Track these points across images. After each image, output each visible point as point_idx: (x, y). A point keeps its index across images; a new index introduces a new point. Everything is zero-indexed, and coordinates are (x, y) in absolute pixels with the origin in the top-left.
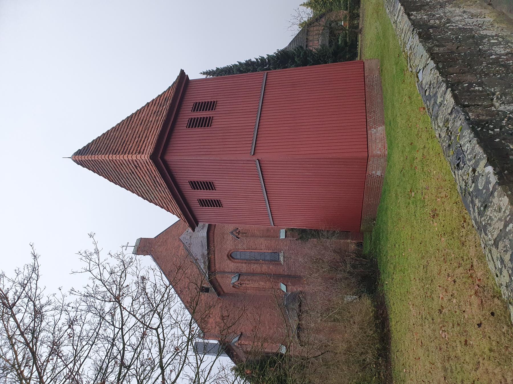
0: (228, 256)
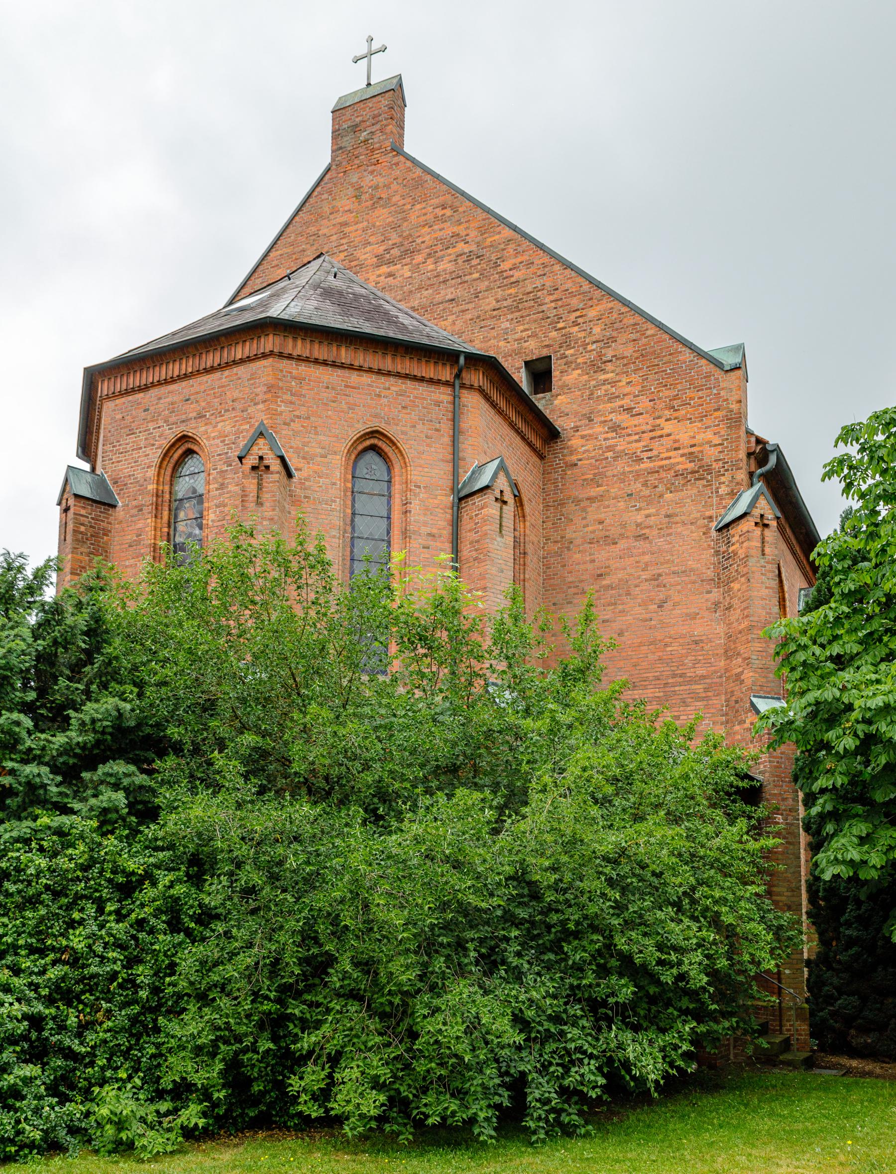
0: (184, 438)
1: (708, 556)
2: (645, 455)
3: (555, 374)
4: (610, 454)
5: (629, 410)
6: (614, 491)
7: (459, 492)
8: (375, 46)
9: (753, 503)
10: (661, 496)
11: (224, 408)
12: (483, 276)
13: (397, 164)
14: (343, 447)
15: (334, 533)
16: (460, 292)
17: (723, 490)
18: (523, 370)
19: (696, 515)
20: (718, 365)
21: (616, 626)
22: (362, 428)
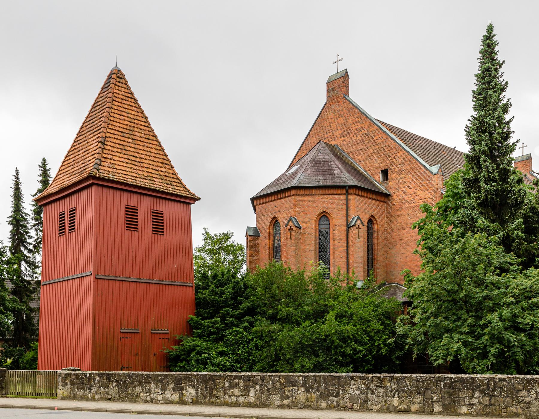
0: (275, 217)
4: (403, 201)
8: (339, 59)
11: (284, 209)
12: (370, 142)
15: (313, 242)
16: (363, 147)
21: (405, 255)
22: (320, 211)
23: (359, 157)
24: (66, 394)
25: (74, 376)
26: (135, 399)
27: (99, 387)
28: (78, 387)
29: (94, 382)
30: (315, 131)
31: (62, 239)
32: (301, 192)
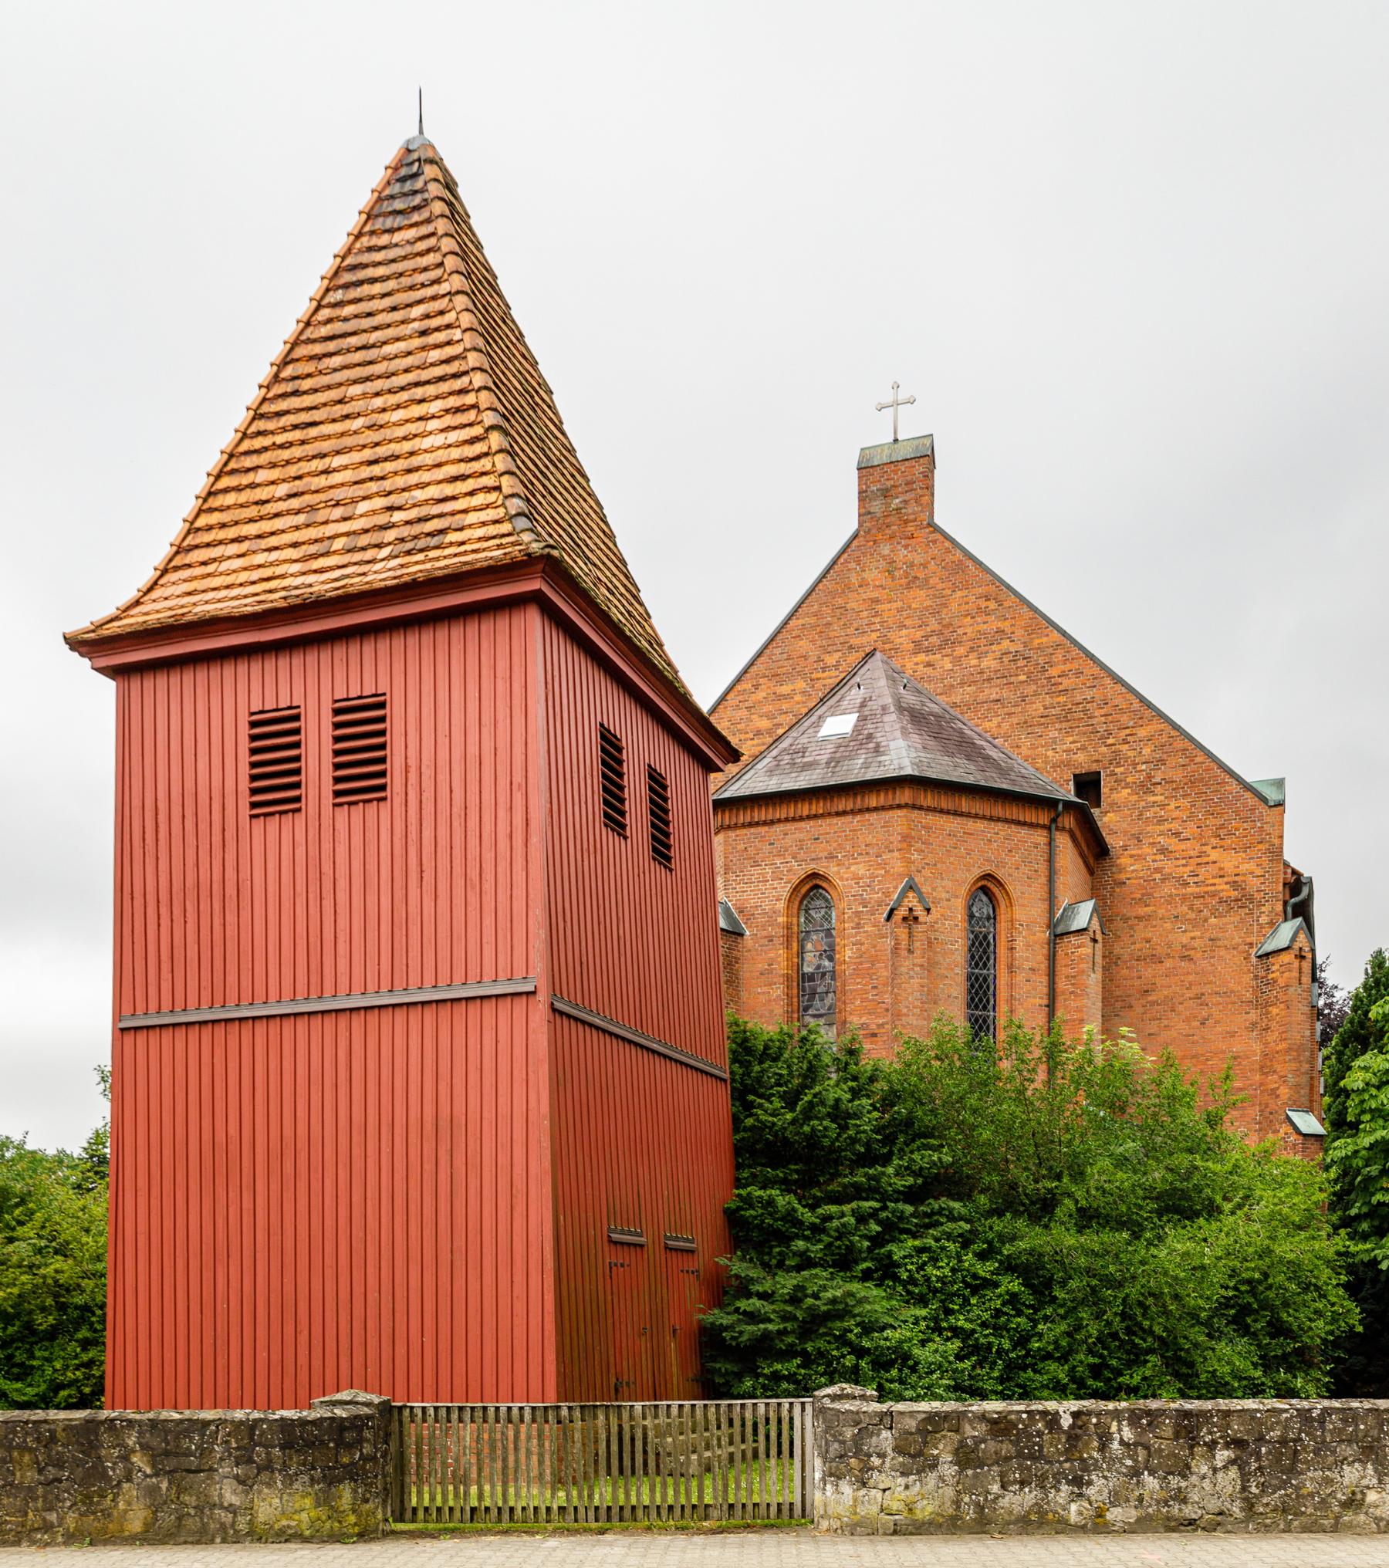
0: (814, 875)
1: (1247, 978)
2: (1191, 880)
3: (1104, 790)
4: (1158, 876)
5: (1177, 834)
6: (1161, 912)
7: (1055, 926)
8: (902, 396)
9: (1294, 939)
10: (1206, 920)
12: (1030, 679)
13: (934, 542)
14: (964, 890)
17: (1264, 919)
18: (1072, 783)
19: (1237, 940)
20: (1264, 800)
22: (977, 872)
23: (988, 725)
24: (926, 1509)
25: (983, 1428)
26: (1337, 1518)
27: (1135, 1472)
28: (1002, 1475)
29: (1103, 1448)
30: (813, 620)
31: (281, 835)
32: (928, 799)
